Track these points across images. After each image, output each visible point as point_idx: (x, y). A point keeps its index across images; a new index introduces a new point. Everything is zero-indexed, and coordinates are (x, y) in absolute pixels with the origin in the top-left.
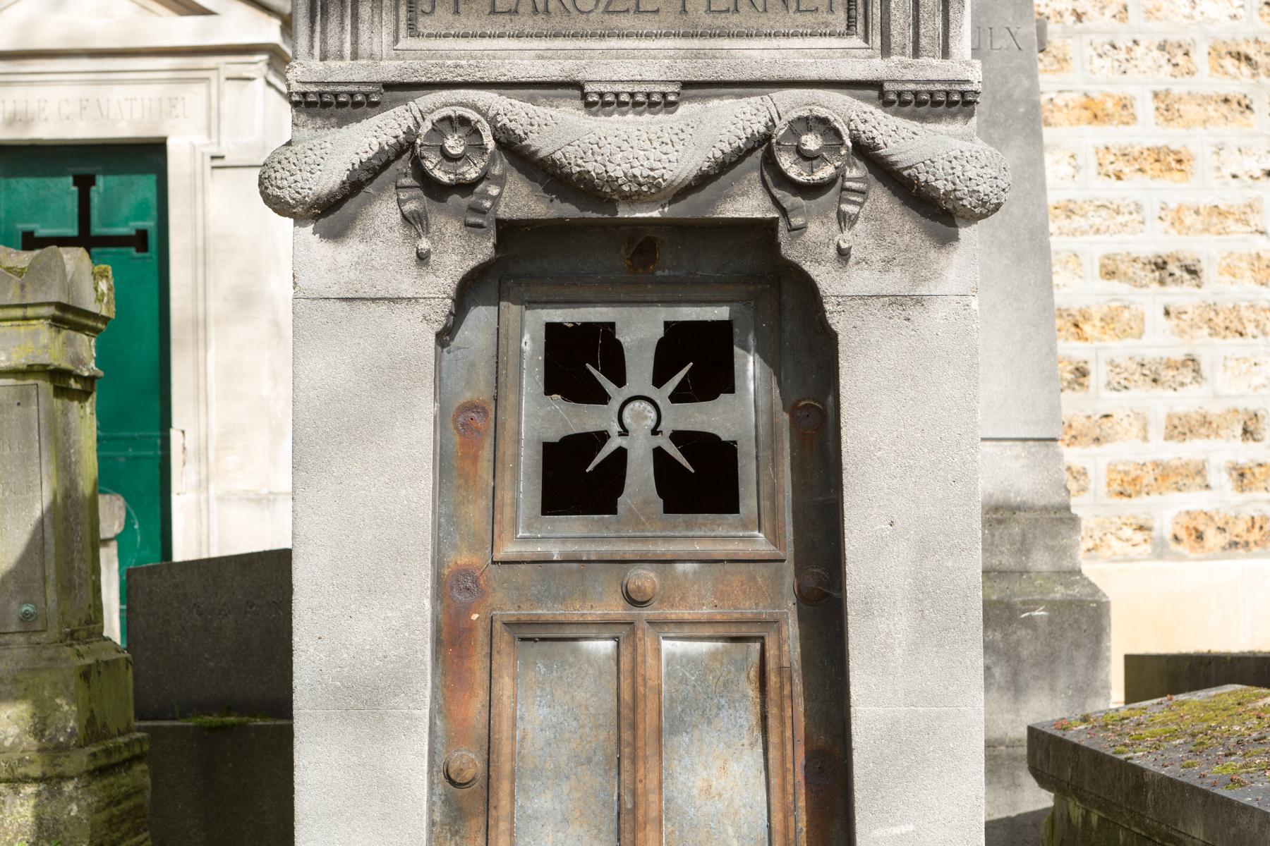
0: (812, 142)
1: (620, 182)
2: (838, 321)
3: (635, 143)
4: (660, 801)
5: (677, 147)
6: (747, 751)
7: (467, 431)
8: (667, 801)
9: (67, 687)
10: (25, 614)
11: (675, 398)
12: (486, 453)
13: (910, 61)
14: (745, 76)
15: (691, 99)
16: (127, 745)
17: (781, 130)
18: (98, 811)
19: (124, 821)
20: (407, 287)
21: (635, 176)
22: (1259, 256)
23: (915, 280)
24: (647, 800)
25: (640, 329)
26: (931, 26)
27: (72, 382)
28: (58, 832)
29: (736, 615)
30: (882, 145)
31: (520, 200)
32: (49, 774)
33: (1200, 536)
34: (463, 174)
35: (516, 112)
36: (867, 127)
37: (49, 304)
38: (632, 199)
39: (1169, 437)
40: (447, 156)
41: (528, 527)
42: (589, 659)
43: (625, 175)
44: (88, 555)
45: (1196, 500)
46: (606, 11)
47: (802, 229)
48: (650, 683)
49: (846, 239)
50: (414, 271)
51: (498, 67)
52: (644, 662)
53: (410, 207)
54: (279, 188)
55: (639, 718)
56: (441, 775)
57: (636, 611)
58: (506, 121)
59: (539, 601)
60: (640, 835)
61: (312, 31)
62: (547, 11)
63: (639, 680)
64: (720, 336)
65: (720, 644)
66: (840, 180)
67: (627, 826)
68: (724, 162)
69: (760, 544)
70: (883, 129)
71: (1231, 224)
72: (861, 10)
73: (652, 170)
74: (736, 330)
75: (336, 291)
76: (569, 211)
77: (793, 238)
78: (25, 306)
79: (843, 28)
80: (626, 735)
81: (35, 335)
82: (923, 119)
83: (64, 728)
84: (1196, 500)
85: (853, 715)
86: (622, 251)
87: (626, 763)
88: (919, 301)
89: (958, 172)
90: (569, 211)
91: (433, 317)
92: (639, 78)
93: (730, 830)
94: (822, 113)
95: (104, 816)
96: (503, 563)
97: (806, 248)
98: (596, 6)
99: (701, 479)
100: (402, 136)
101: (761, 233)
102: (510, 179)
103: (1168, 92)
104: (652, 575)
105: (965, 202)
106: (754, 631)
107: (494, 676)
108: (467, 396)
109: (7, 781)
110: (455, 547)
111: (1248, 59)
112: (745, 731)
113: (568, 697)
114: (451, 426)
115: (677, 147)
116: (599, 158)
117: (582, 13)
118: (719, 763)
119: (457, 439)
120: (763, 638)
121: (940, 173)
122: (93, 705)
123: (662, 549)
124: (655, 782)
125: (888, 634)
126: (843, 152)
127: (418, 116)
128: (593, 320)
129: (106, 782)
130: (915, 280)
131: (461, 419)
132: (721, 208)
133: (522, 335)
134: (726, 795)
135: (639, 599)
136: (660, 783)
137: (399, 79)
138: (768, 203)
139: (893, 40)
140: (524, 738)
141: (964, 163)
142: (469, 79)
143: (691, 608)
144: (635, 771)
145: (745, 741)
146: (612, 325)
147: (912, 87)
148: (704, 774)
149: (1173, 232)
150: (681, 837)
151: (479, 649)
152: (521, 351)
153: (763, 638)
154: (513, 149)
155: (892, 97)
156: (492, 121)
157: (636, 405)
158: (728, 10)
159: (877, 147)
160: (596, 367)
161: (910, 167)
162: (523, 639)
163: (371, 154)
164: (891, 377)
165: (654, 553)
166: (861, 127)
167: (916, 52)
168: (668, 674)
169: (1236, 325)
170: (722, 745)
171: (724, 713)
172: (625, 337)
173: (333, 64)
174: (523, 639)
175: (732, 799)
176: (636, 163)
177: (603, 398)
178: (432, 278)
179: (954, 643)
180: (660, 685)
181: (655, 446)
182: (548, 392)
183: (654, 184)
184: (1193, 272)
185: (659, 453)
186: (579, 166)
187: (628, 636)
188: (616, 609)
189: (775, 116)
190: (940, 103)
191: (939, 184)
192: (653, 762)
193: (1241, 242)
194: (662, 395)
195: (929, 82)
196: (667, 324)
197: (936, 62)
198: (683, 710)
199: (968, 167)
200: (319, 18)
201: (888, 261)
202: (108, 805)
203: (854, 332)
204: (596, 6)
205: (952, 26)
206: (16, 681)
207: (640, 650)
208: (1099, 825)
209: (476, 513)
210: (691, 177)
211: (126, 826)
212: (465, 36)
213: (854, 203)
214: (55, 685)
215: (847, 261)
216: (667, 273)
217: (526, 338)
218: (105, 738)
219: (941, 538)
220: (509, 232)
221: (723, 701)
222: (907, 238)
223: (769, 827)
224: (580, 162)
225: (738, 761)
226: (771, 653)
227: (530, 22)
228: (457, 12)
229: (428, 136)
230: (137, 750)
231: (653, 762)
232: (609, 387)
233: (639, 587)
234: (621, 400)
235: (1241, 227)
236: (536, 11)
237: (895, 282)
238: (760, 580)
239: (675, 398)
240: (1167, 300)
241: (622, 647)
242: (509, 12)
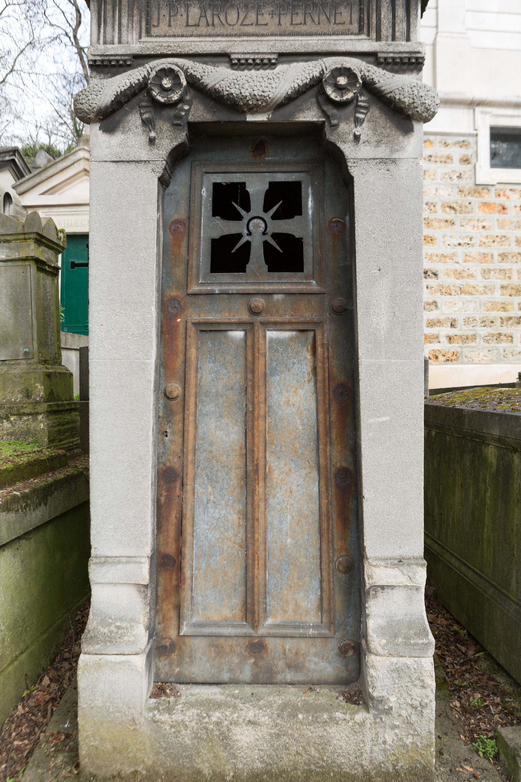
0: (342, 81)
1: (248, 98)
2: (354, 171)
3: (255, 79)
4: (266, 407)
5: (276, 81)
6: (306, 384)
7: (174, 233)
8: (269, 407)
9: (40, 379)
10: (25, 352)
11: (274, 217)
12: (184, 244)
13: (391, 42)
14: (310, 50)
15: (283, 63)
16: (68, 404)
17: (327, 74)
18: (52, 427)
19: (66, 432)
20: (144, 155)
21: (255, 95)
22: (456, 270)
23: (392, 151)
24: (259, 406)
25: (257, 187)
26: (401, 27)
27: (47, 267)
28: (36, 434)
29: (302, 319)
30: (377, 82)
31: (198, 112)
32: (32, 412)
33: (437, 358)
34: (171, 98)
35: (197, 68)
36: (370, 73)
37: (34, 233)
38: (255, 109)
39: (428, 326)
40: (164, 90)
41: (204, 279)
42: (232, 340)
43: (250, 94)
44: (56, 334)
45: (436, 346)
46: (242, 24)
47: (336, 126)
48: (261, 352)
49: (358, 131)
50: (148, 148)
51: (188, 47)
52: (258, 341)
53: (145, 116)
54: (81, 104)
55: (256, 367)
56: (163, 394)
57: (255, 318)
58: (192, 71)
59: (209, 313)
60: (256, 423)
61: (99, 32)
62: (213, 25)
63: (256, 350)
64: (296, 186)
65: (294, 333)
66: (355, 101)
67: (250, 419)
68: (299, 90)
69: (314, 286)
70: (378, 74)
71: (447, 260)
72: (366, 22)
73: (263, 92)
74: (303, 186)
75: (110, 158)
76: (223, 116)
77: (332, 131)
78: (25, 234)
79: (357, 31)
80: (250, 376)
81: (29, 245)
82: (397, 72)
83: (39, 395)
84: (436, 346)
85: (360, 363)
86: (249, 148)
87: (249, 389)
88: (394, 161)
89: (416, 93)
90: (223, 116)
91: (157, 170)
92: (257, 51)
93: (298, 421)
94: (348, 66)
95: (56, 429)
96: (192, 294)
97: (338, 135)
98: (237, 22)
99: (285, 256)
100: (141, 79)
101: (314, 133)
102: (194, 102)
103: (428, 218)
104: (262, 300)
105: (419, 109)
106: (310, 327)
107: (188, 348)
108: (176, 217)
109: (17, 415)
110: (169, 288)
111: (454, 208)
112: (306, 374)
113: (222, 358)
114: (168, 231)
115: (276, 81)
116: (237, 86)
117: (230, 25)
118: (294, 389)
119: (171, 237)
120: (314, 330)
121: (406, 94)
122: (52, 388)
123: (267, 288)
124: (263, 398)
125: (377, 324)
126: (358, 85)
127: (150, 70)
128: (235, 181)
129: (57, 416)
130: (392, 151)
131: (173, 228)
132: (297, 116)
133: (202, 188)
134: (297, 405)
135: (256, 312)
136: (266, 399)
137: (140, 53)
138: (320, 114)
139: (382, 34)
140: (201, 377)
141: (418, 88)
142: (175, 52)
143: (281, 316)
144: (254, 393)
145: (306, 380)
146: (244, 184)
147: (391, 55)
148: (286, 395)
149: (429, 262)
150: (275, 424)
151: (180, 335)
152: (201, 195)
153: (314, 330)
154: (195, 85)
155: (382, 60)
156: (186, 72)
157: (255, 221)
158: (301, 24)
159: (375, 83)
160: (237, 204)
161: (391, 92)
162: (202, 331)
163: (126, 87)
164: (380, 198)
165: (263, 290)
166: (367, 74)
167: (394, 39)
168: (270, 347)
169: (449, 291)
170: (295, 381)
171: (296, 366)
172: (250, 189)
173: (109, 46)
174: (202, 331)
175: (299, 407)
176: (255, 88)
177: (239, 218)
178: (156, 151)
179: (410, 328)
180: (266, 353)
181: (264, 240)
182: (214, 214)
183: (263, 99)
184: (435, 275)
185: (266, 244)
186: (227, 91)
187: (251, 329)
188: (245, 316)
189: (324, 68)
190: (405, 64)
191: (406, 100)
192: (262, 389)
193: (450, 265)
194: (268, 216)
195: (400, 53)
196: (270, 183)
197: (404, 43)
198: (277, 365)
199: (420, 90)
200: (102, 26)
201: (379, 142)
202: (58, 425)
203: (362, 176)
204: (237, 22)
205: (412, 26)
206: (21, 377)
207: (256, 336)
208: (436, 435)
209: (179, 272)
210: (282, 97)
211: (67, 434)
212: (174, 36)
213: (362, 113)
214: (35, 378)
215: (359, 142)
216: (270, 158)
217: (204, 189)
218: (59, 401)
219: (404, 277)
220: (195, 130)
221: (295, 361)
222: (388, 130)
223: (317, 420)
224: (228, 89)
225: (302, 388)
226: (319, 337)
227: (205, 30)
228: (170, 26)
229: (154, 78)
230: (73, 407)
231: (262, 389)
232: (243, 212)
233: (256, 306)
234: (248, 219)
235: (450, 261)
236: (208, 25)
237: (382, 152)
238: (313, 303)
239: (274, 217)
240: (427, 283)
241: (248, 335)
242: (195, 25)
